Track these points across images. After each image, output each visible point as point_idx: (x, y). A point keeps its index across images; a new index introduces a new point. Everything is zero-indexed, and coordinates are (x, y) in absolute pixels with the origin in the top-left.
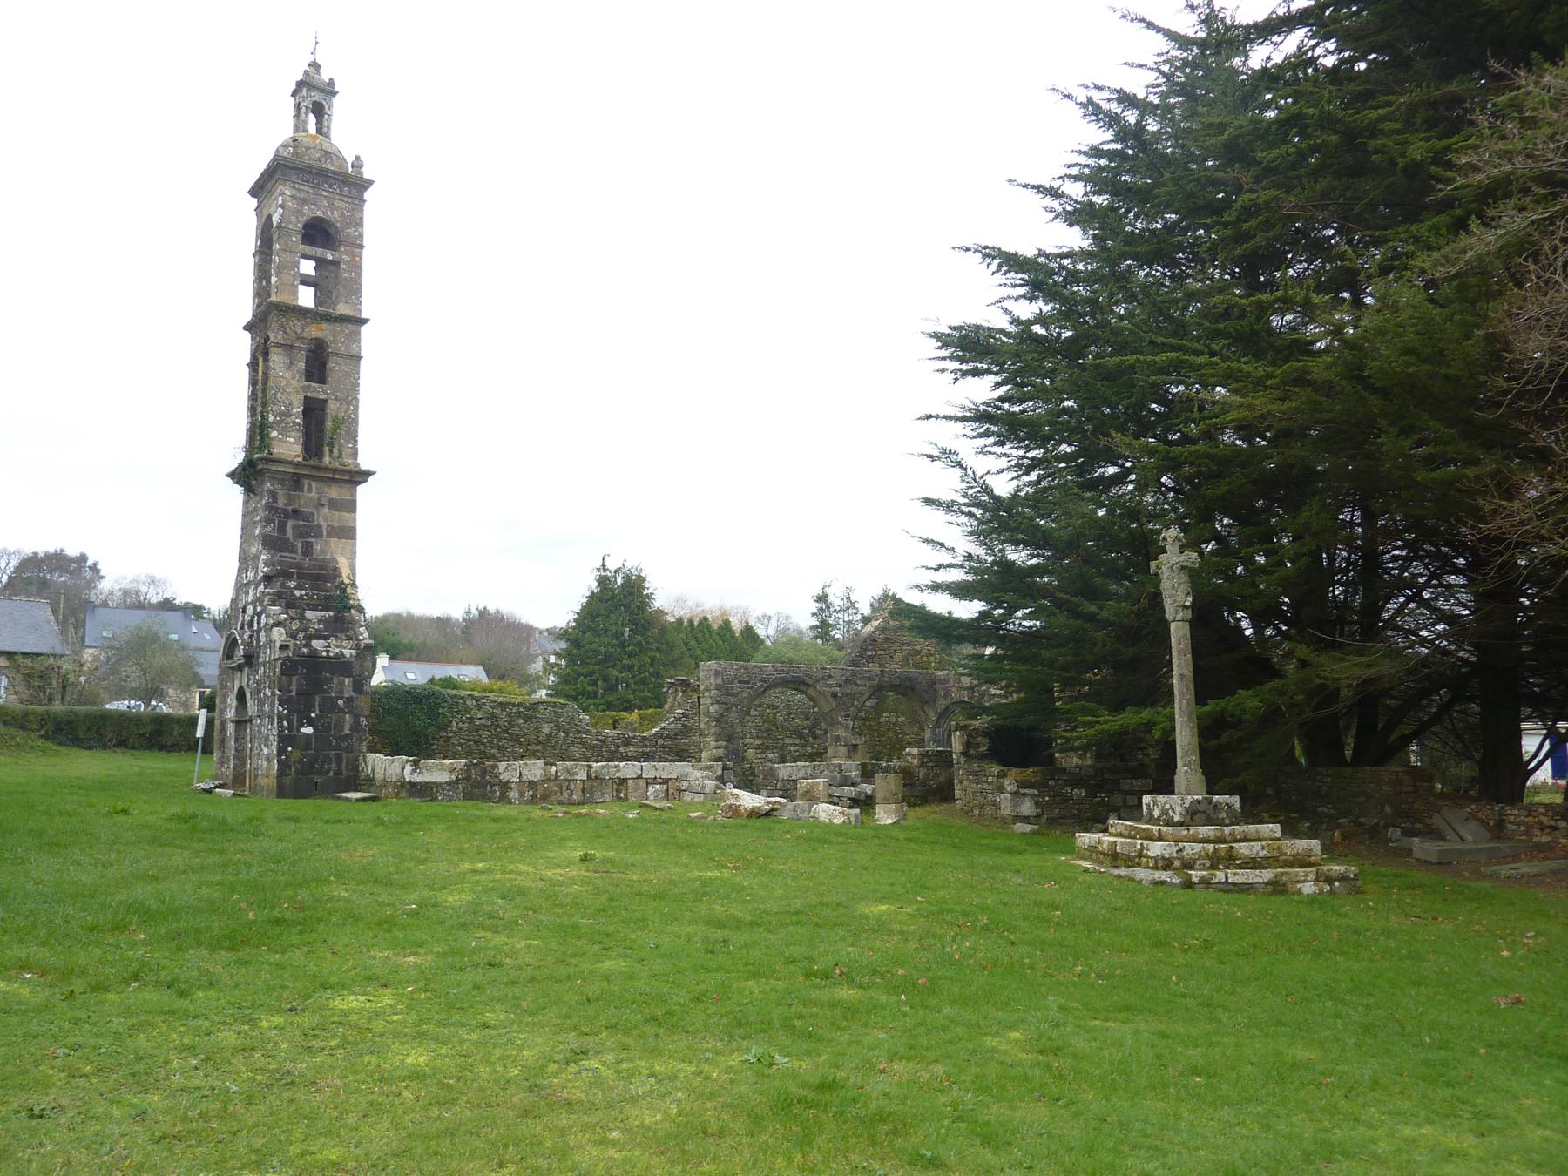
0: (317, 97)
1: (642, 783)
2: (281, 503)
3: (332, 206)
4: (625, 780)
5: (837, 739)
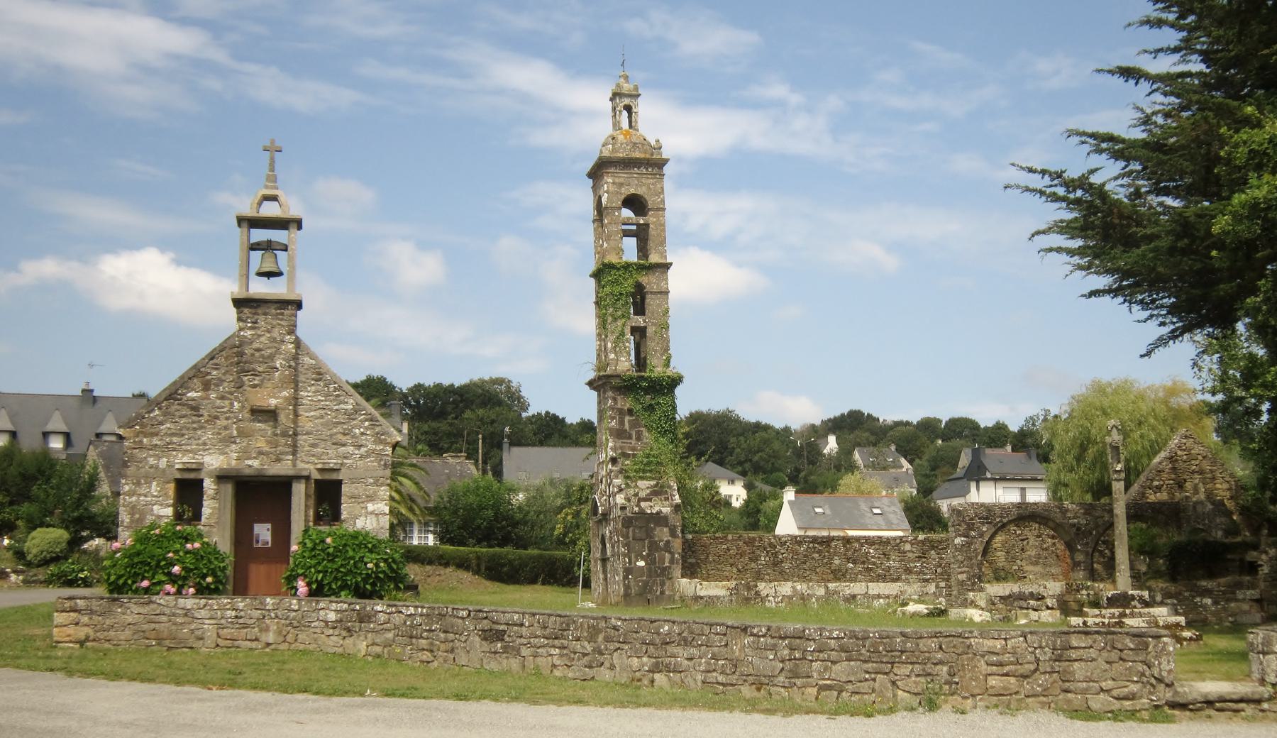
0: (627, 101)
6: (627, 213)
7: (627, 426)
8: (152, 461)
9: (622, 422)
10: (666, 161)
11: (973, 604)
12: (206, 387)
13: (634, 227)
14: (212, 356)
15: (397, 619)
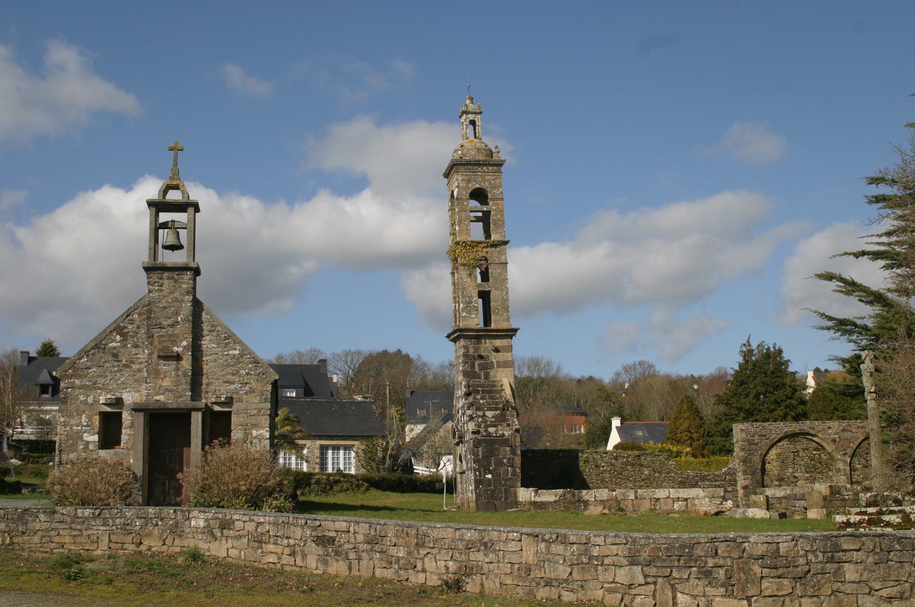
0: (471, 117)
1: (670, 501)
2: (471, 351)
3: (484, 180)
4: (658, 500)
5: (839, 470)
6: (474, 204)
7: (477, 369)
8: (82, 398)
9: (473, 366)
10: (504, 161)
11: (755, 505)
12: (124, 336)
13: (480, 214)
14: (128, 314)
15: (251, 527)
